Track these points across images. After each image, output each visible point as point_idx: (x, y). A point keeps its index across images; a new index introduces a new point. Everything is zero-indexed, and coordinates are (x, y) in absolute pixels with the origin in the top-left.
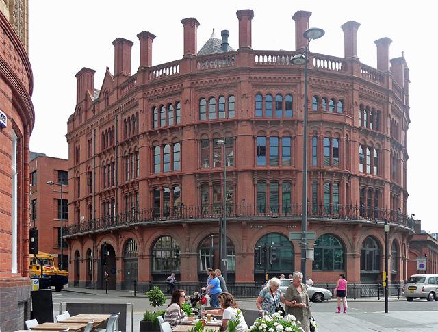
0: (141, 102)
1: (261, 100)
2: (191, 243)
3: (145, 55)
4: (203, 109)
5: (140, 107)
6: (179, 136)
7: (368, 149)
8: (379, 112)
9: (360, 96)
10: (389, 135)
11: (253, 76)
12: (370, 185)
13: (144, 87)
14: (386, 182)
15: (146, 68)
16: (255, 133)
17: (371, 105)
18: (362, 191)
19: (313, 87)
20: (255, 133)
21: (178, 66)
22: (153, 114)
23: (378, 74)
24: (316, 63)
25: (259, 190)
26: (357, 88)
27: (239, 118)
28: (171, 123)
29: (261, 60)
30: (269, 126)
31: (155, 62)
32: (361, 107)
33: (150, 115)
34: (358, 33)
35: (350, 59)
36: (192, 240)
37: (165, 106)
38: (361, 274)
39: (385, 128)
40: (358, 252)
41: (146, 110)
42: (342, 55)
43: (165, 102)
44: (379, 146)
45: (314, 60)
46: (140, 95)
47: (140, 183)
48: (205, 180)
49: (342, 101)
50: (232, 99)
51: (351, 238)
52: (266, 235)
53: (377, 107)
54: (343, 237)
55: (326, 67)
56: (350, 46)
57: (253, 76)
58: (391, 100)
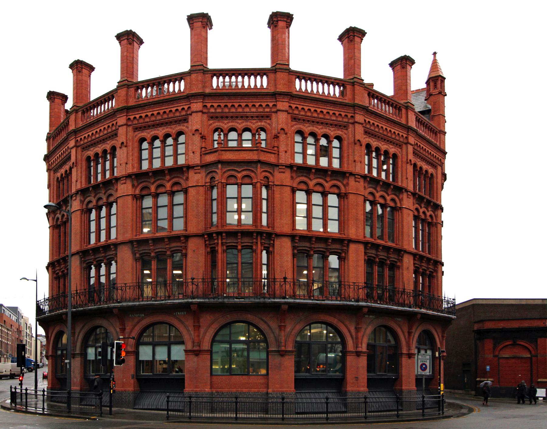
0: (122, 131)
1: (250, 138)
2: (202, 333)
3: (129, 63)
4: (145, 154)
5: (121, 138)
6: (182, 181)
7: (378, 205)
8: (395, 156)
9: (366, 132)
10: (411, 188)
11: (132, 117)
12: (382, 254)
13: (127, 109)
14: (406, 252)
15: (129, 82)
16: (137, 192)
17: (384, 147)
18: (369, 262)
19: (295, 119)
20: (137, 192)
21: (183, 82)
22: (141, 150)
23: (399, 103)
24: (300, 85)
25: (243, 261)
26: (362, 121)
27: (191, 163)
28: (169, 162)
29: (171, 90)
30: (168, 177)
31: (144, 73)
32: (368, 146)
33: (136, 150)
34: (363, 45)
35: (352, 80)
36: (202, 330)
37: (149, 140)
38: (369, 380)
39: (404, 178)
40: (364, 348)
41: (130, 144)
42: (339, 74)
43: (161, 132)
44: (396, 203)
45: (297, 81)
46: (121, 120)
47: (352, 247)
48: (144, 249)
49: (339, 138)
50: (182, 139)
51: (406, 329)
52: (153, 325)
53: (392, 150)
54: (263, 326)
55: (326, 93)
56: (352, 61)
57: (132, 117)
58: (412, 140)
